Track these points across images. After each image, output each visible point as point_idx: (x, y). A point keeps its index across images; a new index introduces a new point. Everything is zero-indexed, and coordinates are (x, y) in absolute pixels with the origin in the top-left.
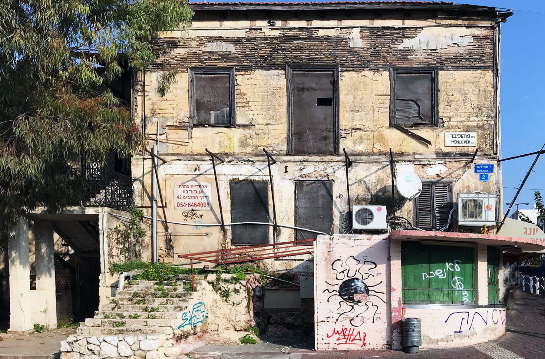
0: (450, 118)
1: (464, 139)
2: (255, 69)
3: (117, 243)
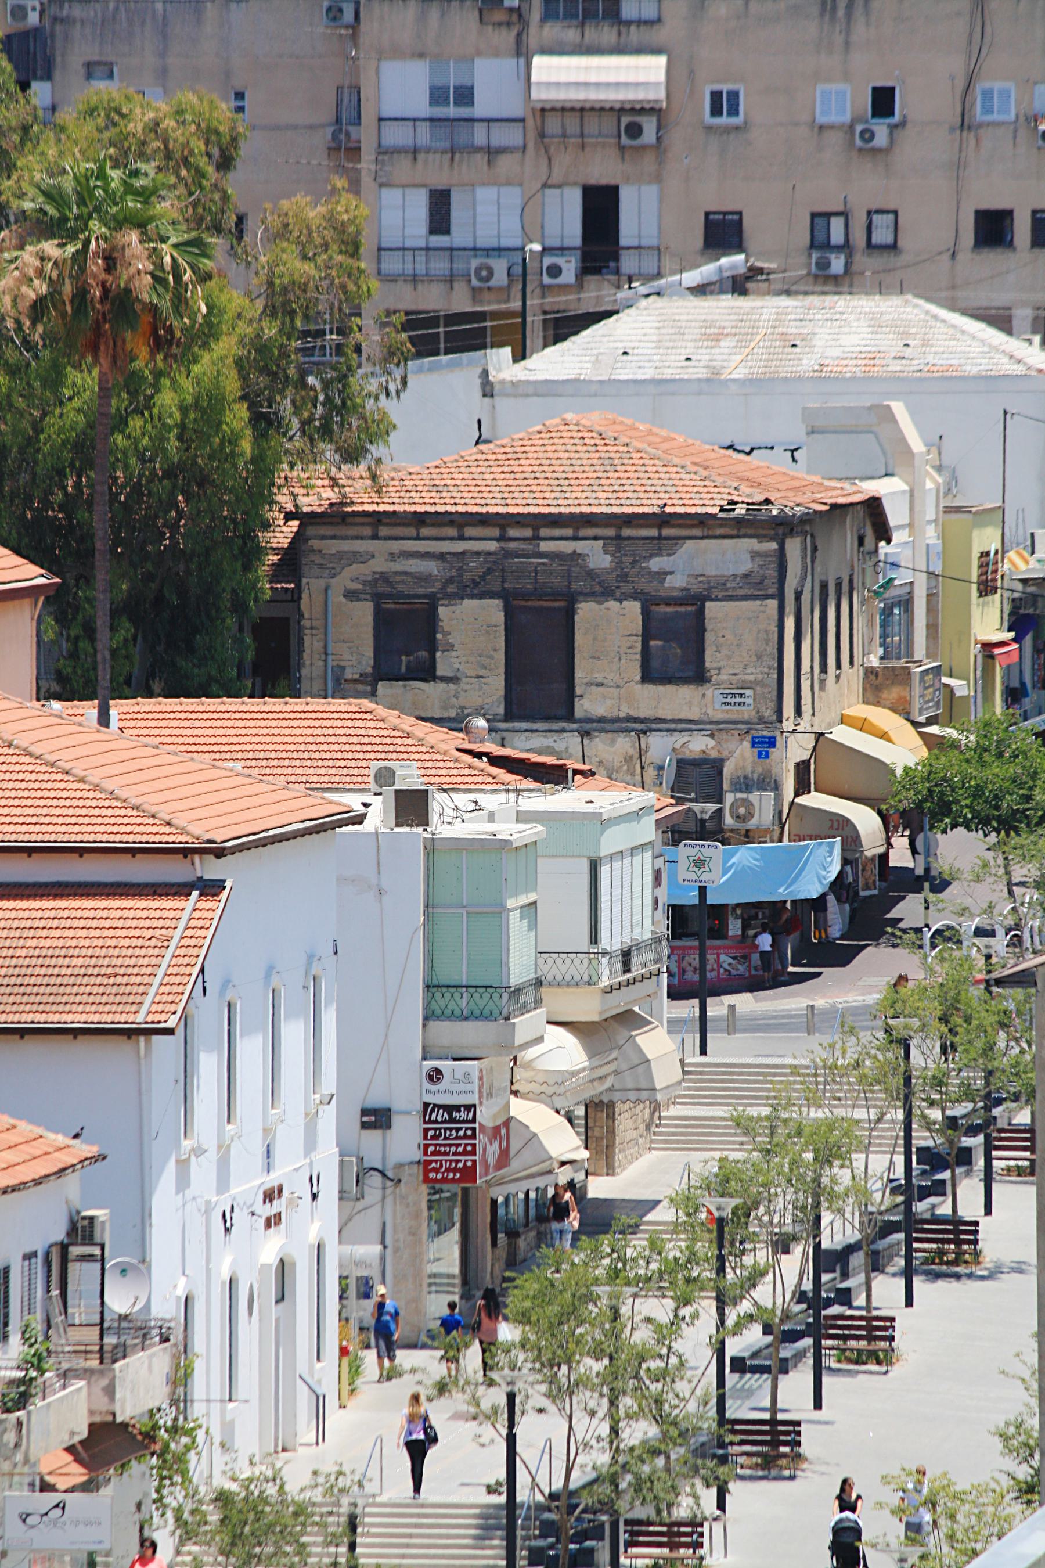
0: (719, 669)
1: (738, 700)
2: (462, 599)
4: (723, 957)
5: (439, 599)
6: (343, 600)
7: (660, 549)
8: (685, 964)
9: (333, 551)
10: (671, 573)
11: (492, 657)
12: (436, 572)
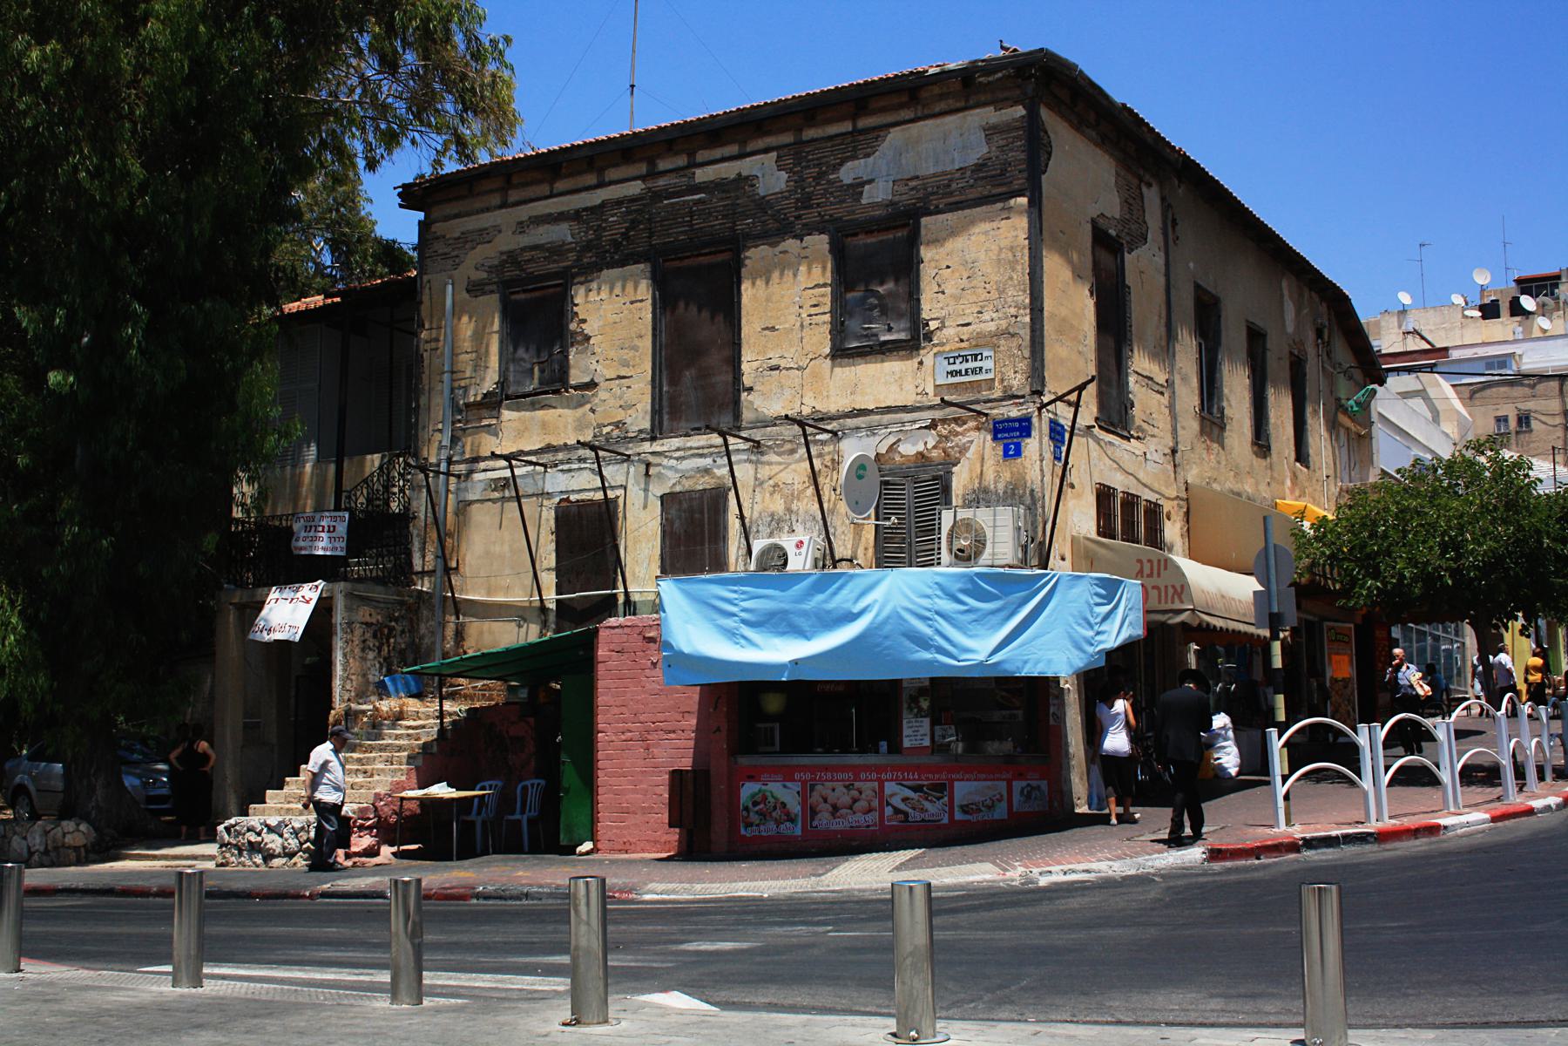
1: (971, 365)
3: (363, 650)
4: (890, 788)
5: (574, 276)
6: (466, 296)
7: (855, 149)
8: (815, 798)
9: (457, 235)
10: (870, 182)
11: (635, 348)
12: (570, 239)
